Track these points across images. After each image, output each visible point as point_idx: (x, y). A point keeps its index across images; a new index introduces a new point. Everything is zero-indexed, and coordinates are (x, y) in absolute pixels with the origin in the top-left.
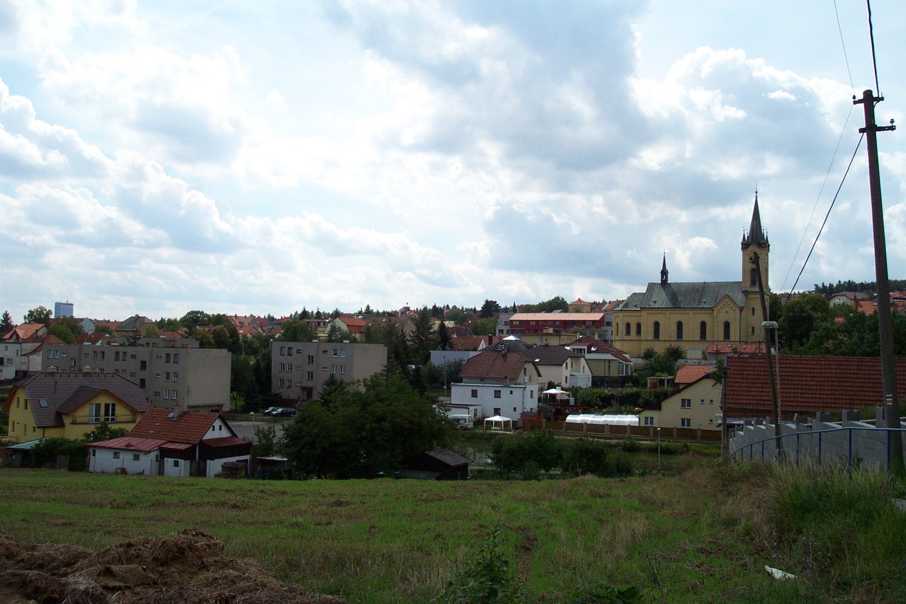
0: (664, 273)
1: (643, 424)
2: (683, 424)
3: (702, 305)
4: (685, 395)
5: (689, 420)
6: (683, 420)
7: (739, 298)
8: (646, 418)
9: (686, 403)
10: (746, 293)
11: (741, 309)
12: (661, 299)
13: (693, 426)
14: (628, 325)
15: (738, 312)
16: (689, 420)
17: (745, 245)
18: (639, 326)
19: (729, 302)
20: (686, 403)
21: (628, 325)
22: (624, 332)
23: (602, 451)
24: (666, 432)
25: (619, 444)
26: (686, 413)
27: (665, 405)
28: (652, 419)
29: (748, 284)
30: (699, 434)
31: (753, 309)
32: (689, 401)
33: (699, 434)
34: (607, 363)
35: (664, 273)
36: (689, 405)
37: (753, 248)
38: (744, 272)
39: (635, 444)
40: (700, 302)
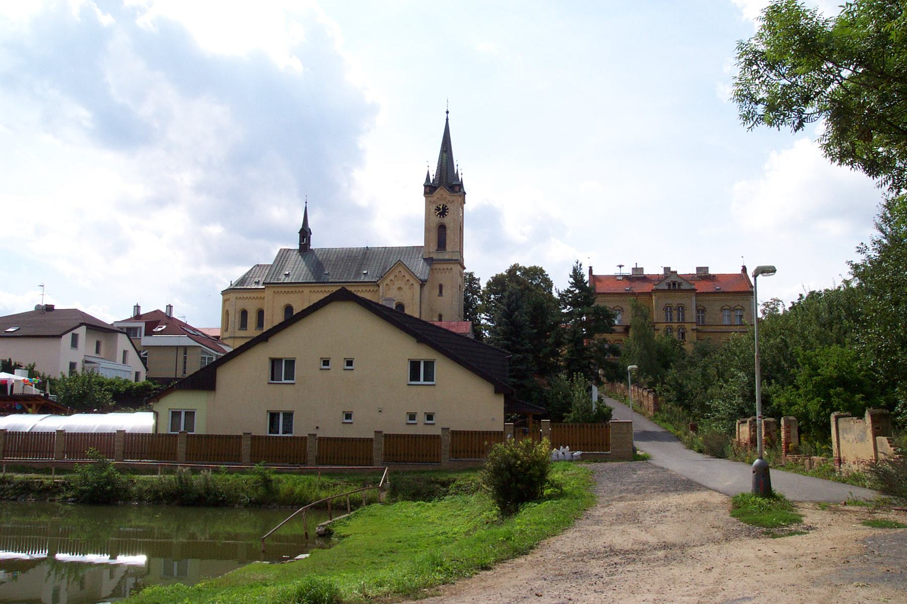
0: (305, 233)
1: (165, 429)
2: (273, 427)
3: (362, 279)
4: (280, 347)
5: (289, 416)
6: (274, 416)
7: (420, 268)
8: (175, 414)
9: (282, 369)
10: (429, 261)
11: (423, 283)
12: (297, 270)
13: (300, 429)
14: (244, 313)
15: (417, 287)
16: (289, 416)
17: (430, 189)
18: (261, 313)
19: (403, 273)
20: (282, 369)
21: (244, 313)
22: (237, 326)
23: (503, 519)
24: (220, 449)
25: (67, 486)
26: (283, 397)
27: (226, 376)
28: (190, 414)
29: (434, 246)
30: (312, 450)
31: (441, 286)
32: (291, 363)
33: (312, 450)
34: (181, 352)
35: (305, 233)
36: (290, 375)
37: (442, 193)
38: (427, 230)
39: (110, 481)
40: (358, 274)
